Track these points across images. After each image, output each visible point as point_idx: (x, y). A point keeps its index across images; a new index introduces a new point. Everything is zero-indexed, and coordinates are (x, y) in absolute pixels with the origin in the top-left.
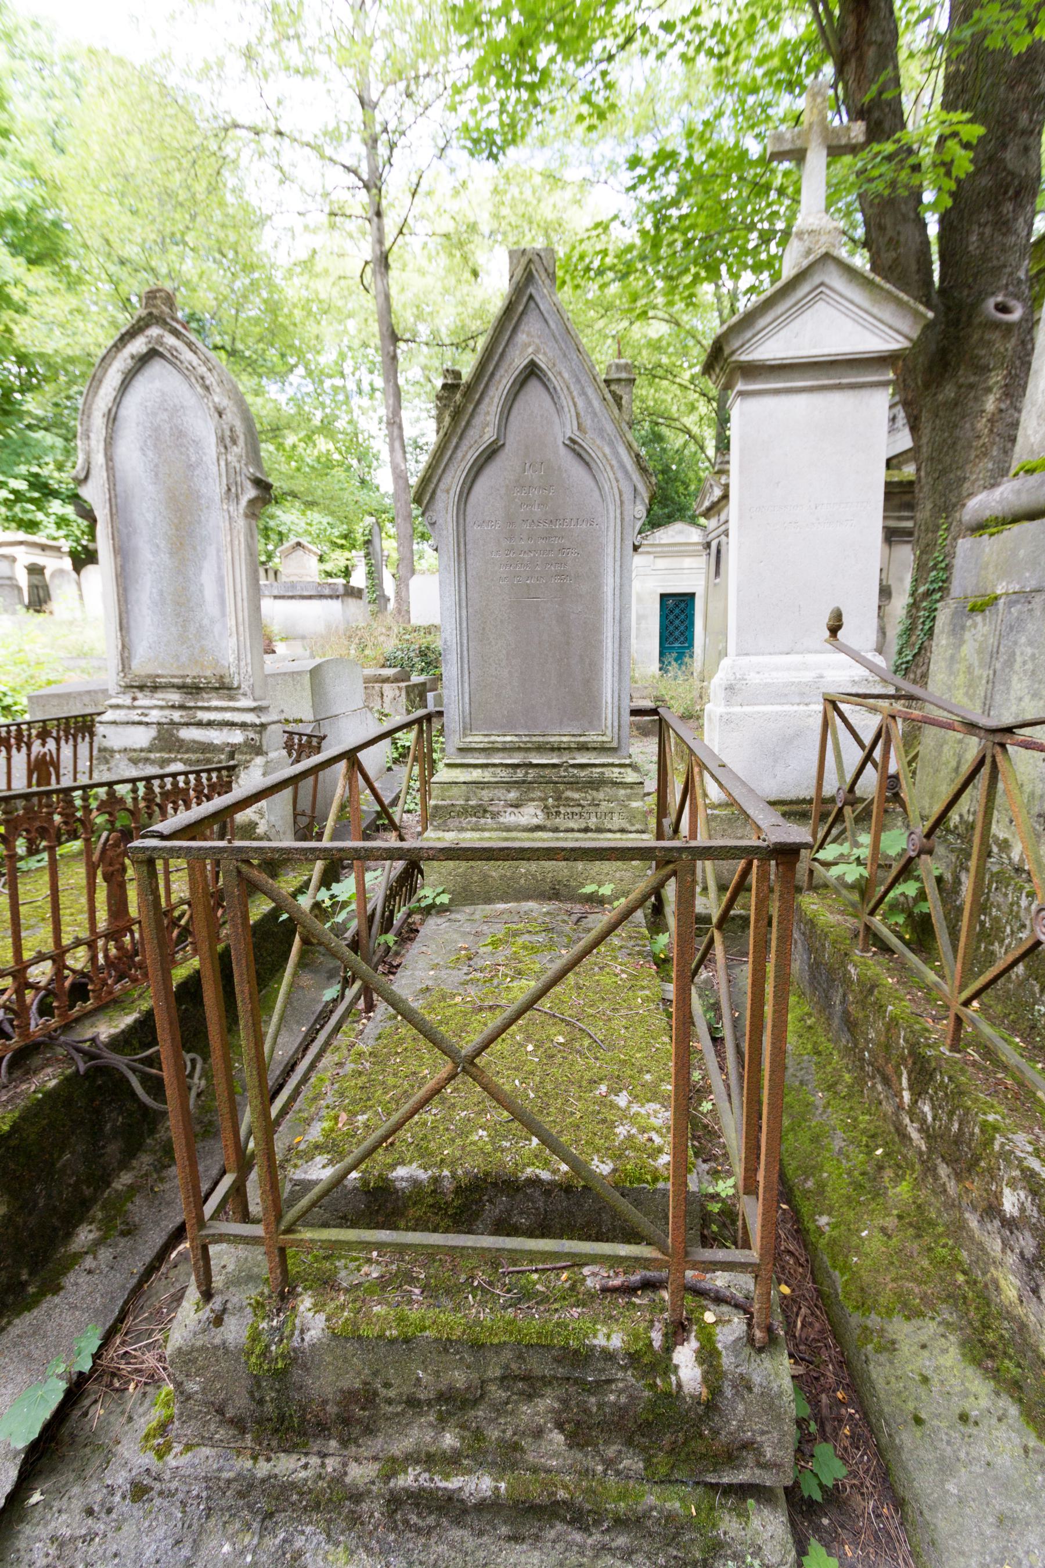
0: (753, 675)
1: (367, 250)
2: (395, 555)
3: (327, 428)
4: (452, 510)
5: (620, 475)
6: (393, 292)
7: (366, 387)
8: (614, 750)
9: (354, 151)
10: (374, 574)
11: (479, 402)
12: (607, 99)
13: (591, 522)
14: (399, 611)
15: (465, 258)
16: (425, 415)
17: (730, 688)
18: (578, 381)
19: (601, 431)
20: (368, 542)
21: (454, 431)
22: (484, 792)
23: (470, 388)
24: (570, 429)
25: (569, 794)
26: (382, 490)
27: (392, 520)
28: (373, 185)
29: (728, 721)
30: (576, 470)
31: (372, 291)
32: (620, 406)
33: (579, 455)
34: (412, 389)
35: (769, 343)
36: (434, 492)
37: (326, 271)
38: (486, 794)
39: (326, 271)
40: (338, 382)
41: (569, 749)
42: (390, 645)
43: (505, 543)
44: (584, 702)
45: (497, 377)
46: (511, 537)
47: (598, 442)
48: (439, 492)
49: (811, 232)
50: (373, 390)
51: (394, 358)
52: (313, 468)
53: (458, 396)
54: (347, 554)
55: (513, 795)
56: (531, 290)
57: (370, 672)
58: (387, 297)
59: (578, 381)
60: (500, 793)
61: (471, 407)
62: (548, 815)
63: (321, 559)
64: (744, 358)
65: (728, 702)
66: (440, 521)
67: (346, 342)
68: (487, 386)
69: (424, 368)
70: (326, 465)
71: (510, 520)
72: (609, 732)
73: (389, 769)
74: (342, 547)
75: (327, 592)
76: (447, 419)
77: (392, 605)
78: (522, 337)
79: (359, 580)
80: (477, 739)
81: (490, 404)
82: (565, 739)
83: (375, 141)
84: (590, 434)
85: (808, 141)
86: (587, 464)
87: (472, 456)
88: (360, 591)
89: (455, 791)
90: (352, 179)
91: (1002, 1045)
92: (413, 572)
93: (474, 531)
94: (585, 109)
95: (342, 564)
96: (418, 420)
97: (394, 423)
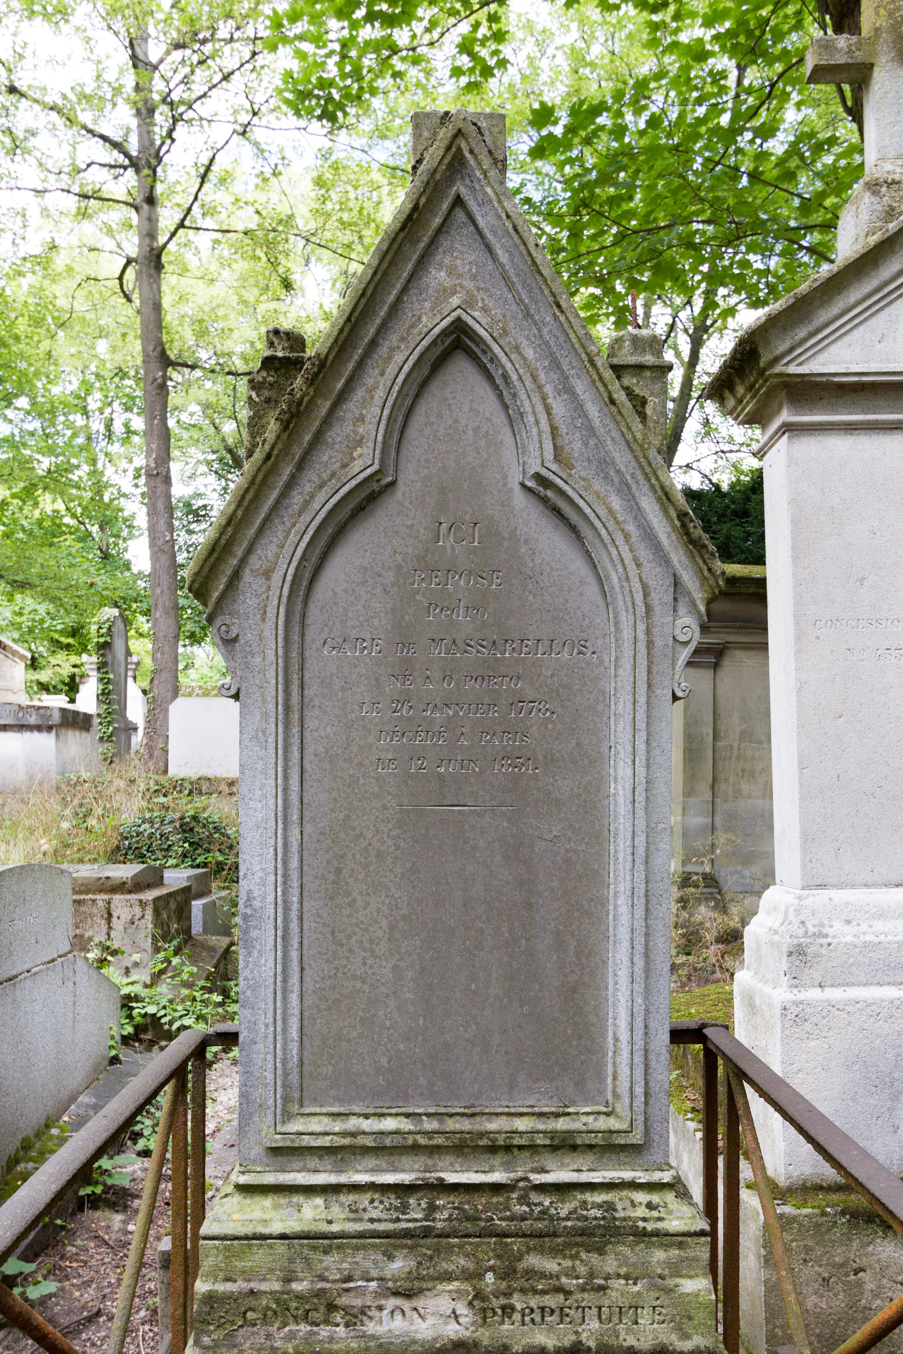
0: (838, 925)
1: (132, 246)
2: (148, 663)
3: (55, 481)
4: (276, 613)
5: (644, 553)
6: (167, 301)
7: (118, 428)
8: (635, 1150)
9: (120, 120)
10: (112, 695)
11: (342, 398)
12: (496, 53)
13: (582, 646)
14: (150, 748)
15: (274, 264)
16: (203, 468)
17: (798, 953)
18: (555, 365)
19: (604, 464)
20: (104, 647)
21: (286, 451)
22: (330, 1260)
23: (325, 366)
24: (538, 458)
25: (534, 1261)
26: (135, 570)
27: (146, 613)
28: (147, 163)
29: (799, 1019)
30: (548, 542)
31: (135, 297)
32: (643, 416)
33: (557, 512)
34: (186, 435)
35: (834, 348)
36: (236, 575)
37: (70, 269)
38: (333, 1264)
39: (70, 269)
40: (79, 420)
41: (532, 1148)
42: (130, 811)
43: (391, 687)
44: (567, 1044)
45: (383, 350)
46: (405, 673)
47: (597, 485)
48: (247, 576)
49: (891, 184)
50: (129, 432)
51: (162, 388)
52: (30, 534)
53: (299, 382)
54: (74, 659)
55: (399, 1265)
56: (460, 188)
57: (86, 872)
58: (157, 307)
59: (555, 365)
60: (367, 1260)
61: (325, 406)
62: (484, 1314)
63: (34, 664)
64: (792, 369)
65: (796, 980)
66: (248, 636)
67: (93, 368)
68: (361, 365)
69: (206, 406)
70: (51, 531)
71: (403, 639)
72: (622, 1107)
73: (114, 1060)
74: (68, 646)
75: (33, 720)
76: (272, 428)
77: (138, 739)
78: (437, 276)
79: (87, 700)
80: (314, 1126)
81: (364, 404)
82: (522, 1124)
83: (151, 111)
84: (580, 470)
85: (875, 54)
86: (573, 529)
87: (323, 502)
88: (88, 718)
89: (259, 1257)
90: (117, 157)
91: (843, 1197)
92: (175, 692)
93: (322, 659)
94: (465, 61)
95: (66, 671)
96: (192, 476)
97: (158, 476)
